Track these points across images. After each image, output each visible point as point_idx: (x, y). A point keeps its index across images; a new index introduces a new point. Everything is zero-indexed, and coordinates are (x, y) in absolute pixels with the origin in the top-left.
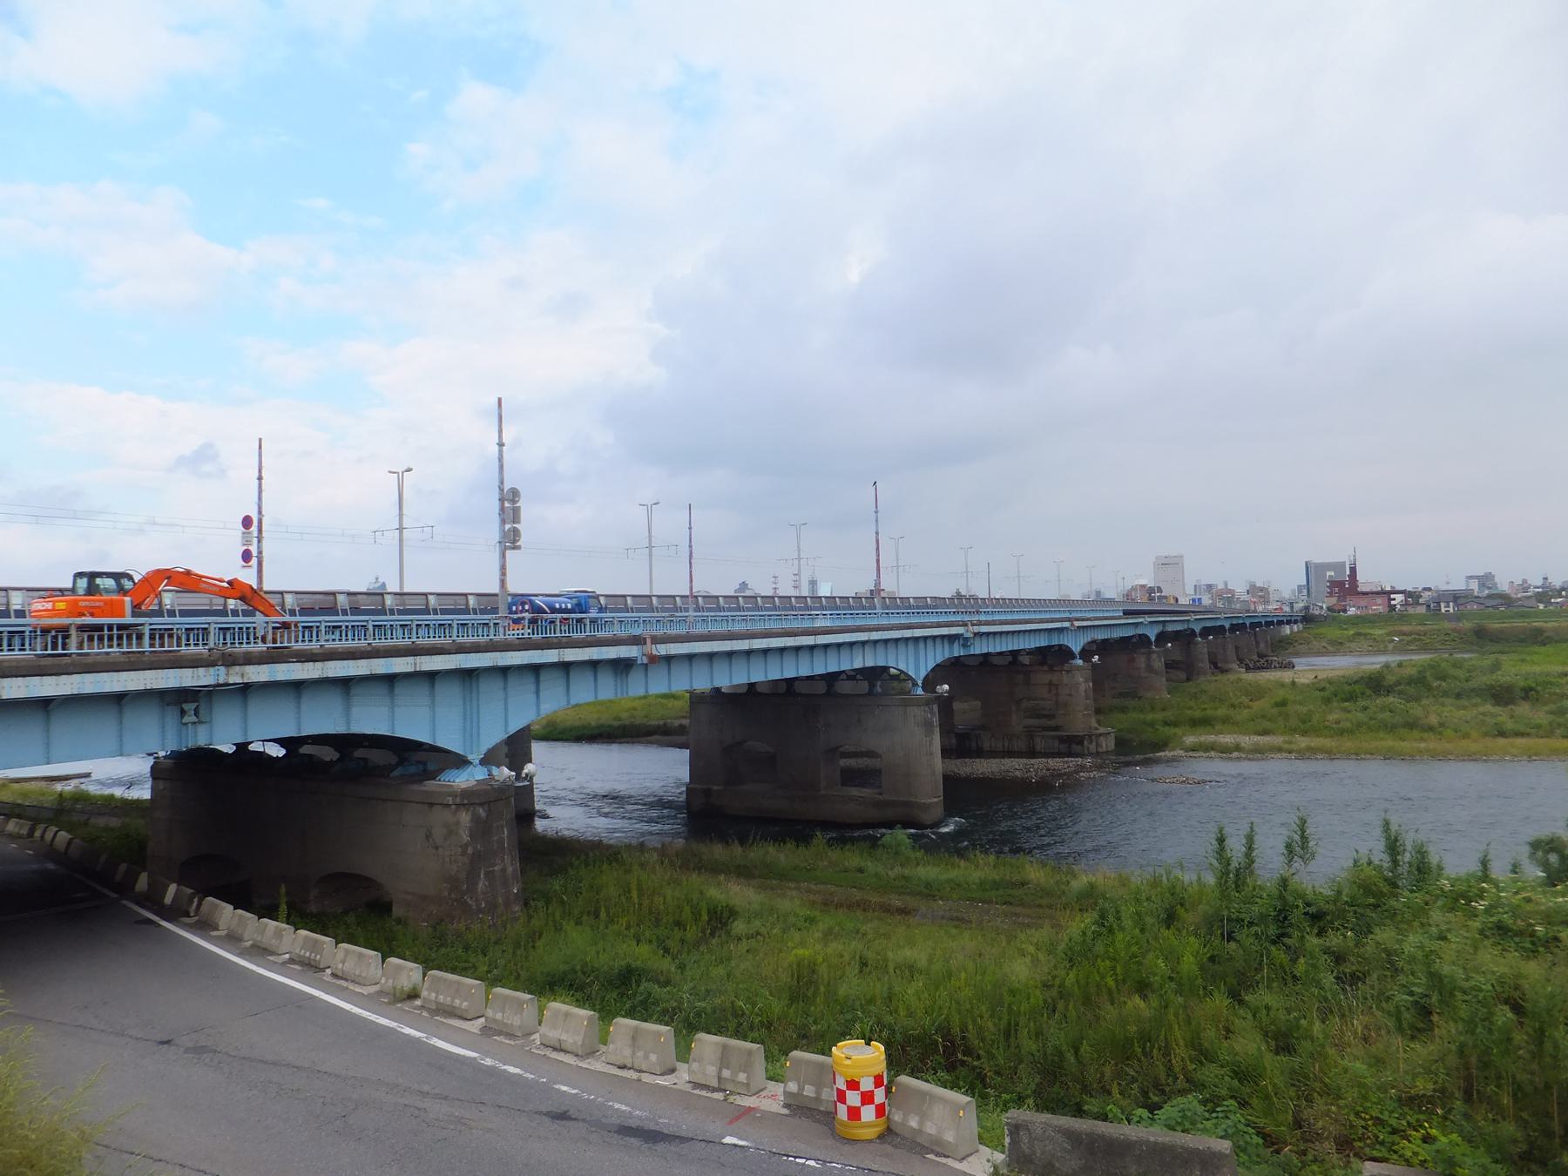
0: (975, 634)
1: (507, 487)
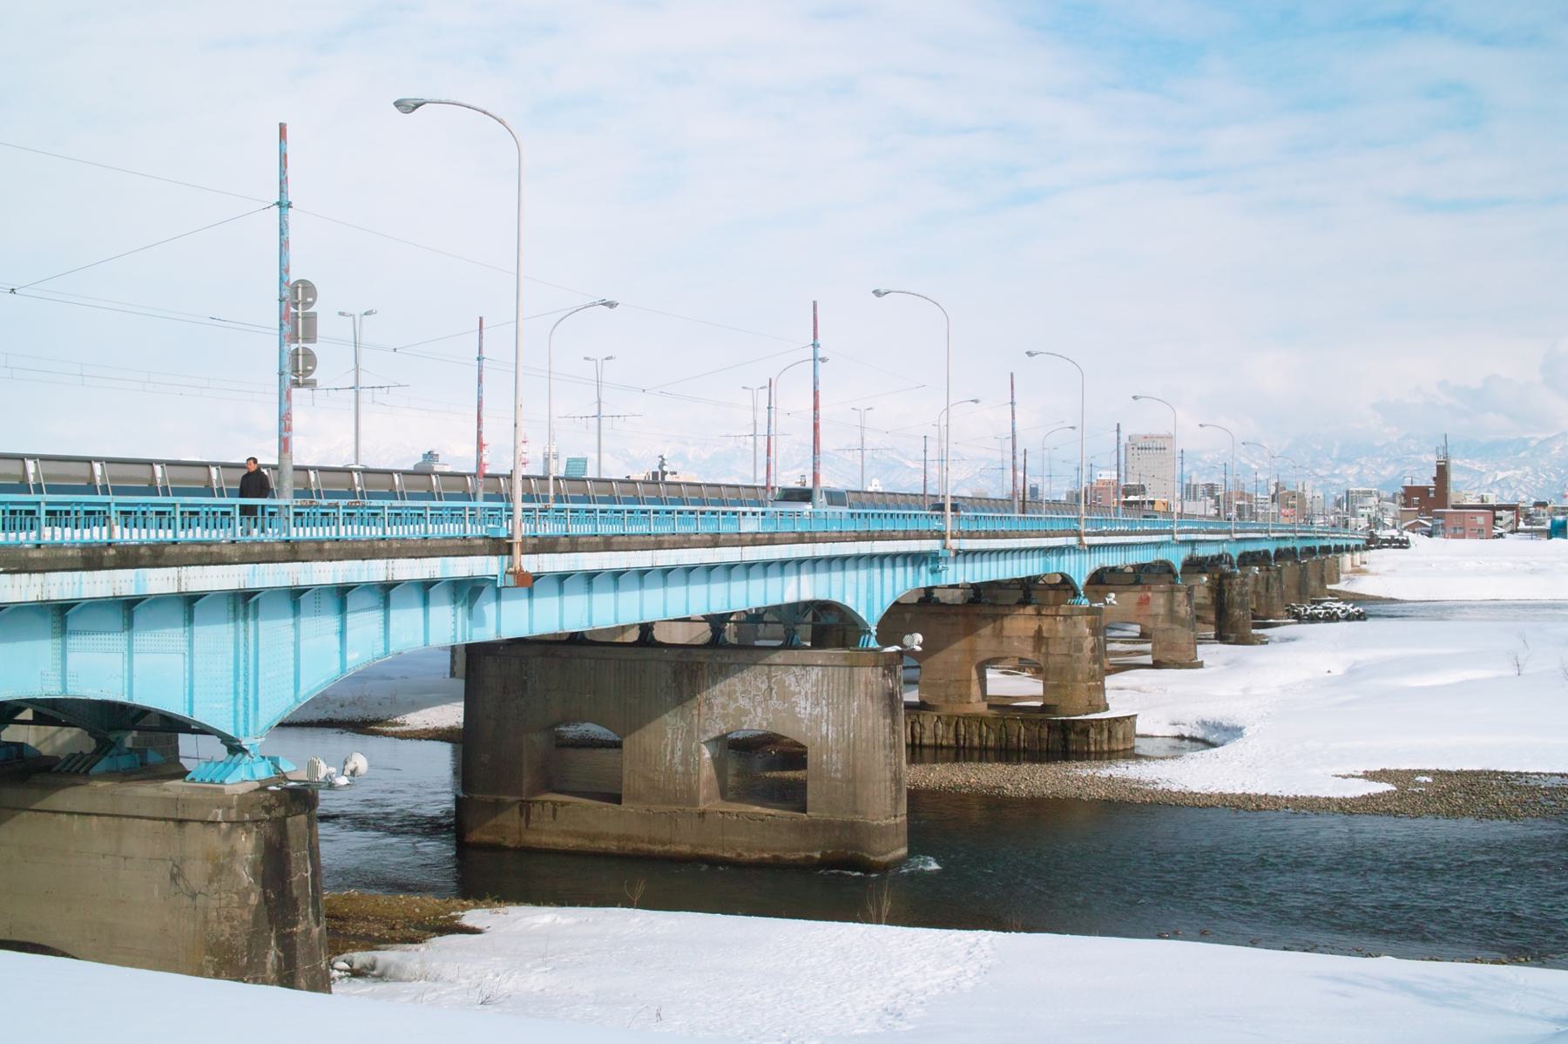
0: (957, 553)
1: (293, 278)
